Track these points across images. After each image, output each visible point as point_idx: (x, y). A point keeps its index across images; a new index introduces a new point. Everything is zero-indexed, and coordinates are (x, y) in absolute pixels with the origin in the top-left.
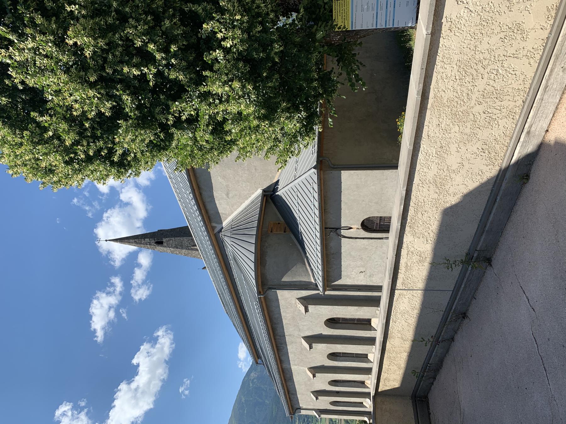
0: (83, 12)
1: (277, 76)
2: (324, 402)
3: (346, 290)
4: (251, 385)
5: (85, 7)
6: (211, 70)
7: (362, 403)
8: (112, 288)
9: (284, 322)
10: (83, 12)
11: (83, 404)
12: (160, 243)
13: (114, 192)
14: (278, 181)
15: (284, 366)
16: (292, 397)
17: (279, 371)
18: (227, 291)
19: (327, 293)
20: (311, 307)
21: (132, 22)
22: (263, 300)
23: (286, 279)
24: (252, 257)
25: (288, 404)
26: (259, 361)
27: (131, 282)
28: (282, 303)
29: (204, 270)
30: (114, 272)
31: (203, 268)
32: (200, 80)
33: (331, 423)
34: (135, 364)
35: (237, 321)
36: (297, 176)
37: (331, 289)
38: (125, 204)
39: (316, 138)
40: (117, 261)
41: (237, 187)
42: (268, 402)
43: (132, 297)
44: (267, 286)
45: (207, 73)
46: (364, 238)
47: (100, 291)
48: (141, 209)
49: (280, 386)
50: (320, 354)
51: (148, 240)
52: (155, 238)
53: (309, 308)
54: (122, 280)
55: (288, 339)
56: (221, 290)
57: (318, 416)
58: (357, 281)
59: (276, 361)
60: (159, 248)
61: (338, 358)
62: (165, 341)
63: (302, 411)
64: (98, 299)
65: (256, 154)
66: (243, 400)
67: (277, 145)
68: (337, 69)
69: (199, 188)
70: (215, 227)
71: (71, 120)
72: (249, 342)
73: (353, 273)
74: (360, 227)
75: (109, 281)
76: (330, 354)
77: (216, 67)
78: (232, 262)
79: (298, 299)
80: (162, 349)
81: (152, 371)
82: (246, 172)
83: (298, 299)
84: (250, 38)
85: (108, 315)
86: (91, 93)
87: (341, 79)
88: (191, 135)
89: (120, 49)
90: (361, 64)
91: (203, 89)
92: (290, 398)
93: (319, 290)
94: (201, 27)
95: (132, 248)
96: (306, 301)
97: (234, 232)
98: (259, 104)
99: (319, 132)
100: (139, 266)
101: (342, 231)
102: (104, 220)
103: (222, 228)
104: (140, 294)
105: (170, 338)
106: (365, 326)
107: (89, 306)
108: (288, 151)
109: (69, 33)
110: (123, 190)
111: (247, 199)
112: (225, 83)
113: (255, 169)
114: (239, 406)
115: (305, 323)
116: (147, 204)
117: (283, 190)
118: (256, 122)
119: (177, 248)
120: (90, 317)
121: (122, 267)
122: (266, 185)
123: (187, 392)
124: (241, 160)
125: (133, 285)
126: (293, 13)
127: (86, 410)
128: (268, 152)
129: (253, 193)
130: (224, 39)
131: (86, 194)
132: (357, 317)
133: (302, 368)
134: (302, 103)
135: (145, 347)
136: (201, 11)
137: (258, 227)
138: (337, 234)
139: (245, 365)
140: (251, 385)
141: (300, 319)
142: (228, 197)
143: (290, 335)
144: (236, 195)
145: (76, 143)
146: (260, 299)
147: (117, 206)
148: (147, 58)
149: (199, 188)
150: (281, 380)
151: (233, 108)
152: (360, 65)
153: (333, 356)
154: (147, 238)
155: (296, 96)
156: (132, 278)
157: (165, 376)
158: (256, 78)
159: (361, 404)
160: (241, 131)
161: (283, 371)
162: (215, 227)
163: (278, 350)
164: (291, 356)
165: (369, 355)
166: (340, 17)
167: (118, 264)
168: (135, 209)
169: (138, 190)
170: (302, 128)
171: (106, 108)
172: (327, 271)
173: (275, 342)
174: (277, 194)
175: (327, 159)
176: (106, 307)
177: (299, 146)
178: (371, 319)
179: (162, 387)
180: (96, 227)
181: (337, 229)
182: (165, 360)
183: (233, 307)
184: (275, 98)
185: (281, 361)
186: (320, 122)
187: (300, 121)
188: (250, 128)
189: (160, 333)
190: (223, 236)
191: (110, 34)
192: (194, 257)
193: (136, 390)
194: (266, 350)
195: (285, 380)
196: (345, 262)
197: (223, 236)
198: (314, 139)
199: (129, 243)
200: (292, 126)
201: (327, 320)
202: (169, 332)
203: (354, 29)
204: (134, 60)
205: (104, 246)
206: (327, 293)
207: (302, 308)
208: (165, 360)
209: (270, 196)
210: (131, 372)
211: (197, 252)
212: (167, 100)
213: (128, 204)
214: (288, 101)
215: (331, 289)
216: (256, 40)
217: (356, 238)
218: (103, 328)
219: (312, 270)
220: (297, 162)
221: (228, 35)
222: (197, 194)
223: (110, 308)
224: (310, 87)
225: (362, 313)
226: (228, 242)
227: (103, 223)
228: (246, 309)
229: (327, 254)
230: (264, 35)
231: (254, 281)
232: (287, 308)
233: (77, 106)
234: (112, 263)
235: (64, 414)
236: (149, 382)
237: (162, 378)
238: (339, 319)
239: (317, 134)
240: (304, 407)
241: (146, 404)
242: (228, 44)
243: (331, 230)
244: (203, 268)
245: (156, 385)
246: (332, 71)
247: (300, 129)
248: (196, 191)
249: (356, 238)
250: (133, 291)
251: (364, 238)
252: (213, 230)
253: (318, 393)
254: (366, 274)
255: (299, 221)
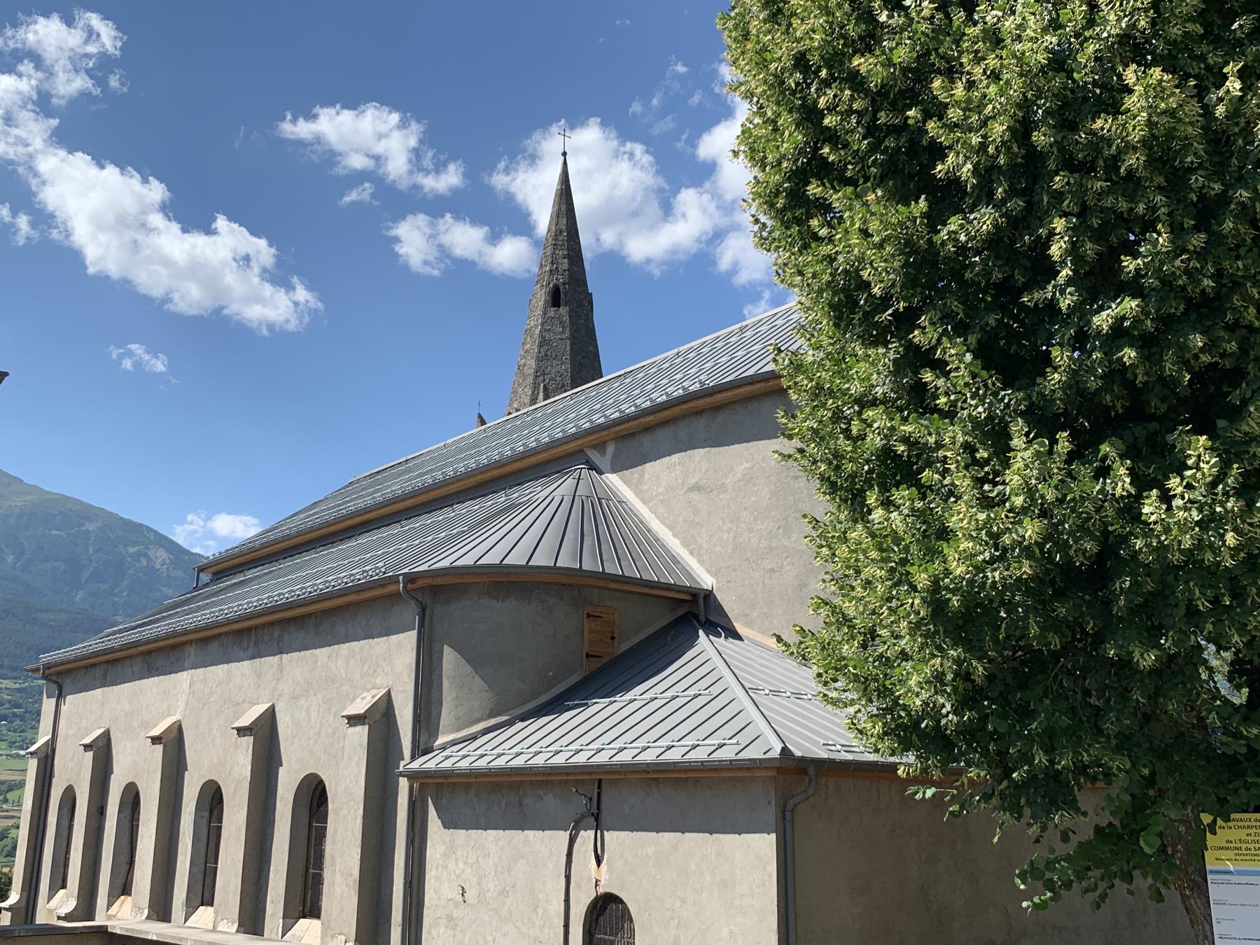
0: (1220, 110)
1: (1055, 642)
2: (74, 770)
3: (410, 841)
4: (132, 550)
5: (1233, 115)
6: (1071, 457)
7: (64, 886)
8: (431, 166)
9: (322, 653)
10: (1220, 110)
11: (114, 82)
12: (555, 298)
13: (703, 173)
14: (738, 637)
15: (191, 651)
16: (98, 672)
17: (175, 634)
18: (418, 483)
19: (404, 783)
20: (362, 732)
21: (1197, 241)
22: (391, 588)
23: (449, 657)
24: (517, 558)
25: (76, 660)
26: (205, 578)
27: (448, 216)
28: (379, 645)
29: (476, 418)
30: (476, 171)
31: (480, 417)
32: (1044, 422)
33: (4, 788)
34: (213, 226)
35: (326, 514)
36: (759, 694)
37: (415, 796)
38: (683, 207)
39: (873, 757)
40: (507, 179)
41: (710, 516)
42: (77, 599)
43: (404, 218)
44: (429, 602)
45: (1064, 443)
46: (567, 901)
47: (424, 132)
48: (647, 246)
49: (133, 636)
50: (222, 760)
51: (566, 266)
52: (569, 285)
53: (358, 728)
54: (455, 191)
55: (271, 661)
56: (418, 467)
57: (32, 749)
58: (437, 878)
59: (207, 627)
60: (540, 297)
61: (206, 814)
62: (274, 307)
63: (53, 701)
64: (403, 125)
65: (828, 577)
66: (90, 527)
67: (853, 638)
68: (1085, 830)
69: (717, 408)
70: (603, 453)
71: (920, 72)
72: (264, 546)
73: (461, 865)
74: (601, 890)
75: (453, 159)
76: (219, 789)
77: (1085, 471)
78: (501, 499)
79: (389, 694)
80: (260, 300)
81: (196, 269)
82: (763, 544)
83: (389, 694)
84: (1170, 572)
85: (356, 152)
86: (998, 129)
87: (1053, 836)
88: (879, 391)
89: (1123, 205)
90: (1104, 896)
91: (1018, 427)
92: (94, 665)
93: (413, 758)
94: (1198, 431)
95: (543, 219)
96: (379, 719)
97: (588, 507)
98: (972, 591)
99: (894, 767)
100: (494, 238)
101: (591, 833)
102: (623, 144)
103: (600, 473)
104: (412, 240)
105: (287, 321)
106: (298, 900)
107: (383, 102)
108: (834, 668)
109: (1156, 72)
110: (706, 197)
111: (685, 545)
112: (1030, 492)
113: (773, 570)
114: (73, 515)
115: (314, 715)
116: (665, 263)
117: (711, 652)
118: (922, 579)
119: (541, 345)
120: (353, 103)
121: (490, 190)
122: (727, 601)
123: (128, 364)
124: (808, 529)
125: (441, 221)
126: (1245, 691)
127: (97, 92)
128: (835, 610)
129: (701, 562)
130: (1166, 498)
131: (696, 99)
132: (327, 874)
133: (181, 703)
134: (984, 719)
135: (261, 249)
136: (1245, 428)
137: (604, 576)
138: (583, 817)
139: (195, 532)
140: (132, 550)
141: (329, 699)
142: (691, 489)
143: (281, 668)
144: (695, 512)
145: (856, 81)
146: (394, 580)
147: (662, 182)
148: (1100, 281)
149: (717, 408)
150: (148, 642)
151: (962, 516)
152: (1099, 891)
153: (212, 798)
154: (570, 264)
155: (1002, 700)
156: (458, 217)
157: (181, 305)
158: (1052, 582)
159: (60, 882)
160: (897, 540)
161: (174, 647)
162: (603, 453)
163: (240, 632)
164: (219, 671)
165: (209, 908)
166: (1242, 834)
167: (499, 180)
168: (653, 228)
169: (704, 238)
170: (909, 714)
171: (957, 165)
172: (468, 786)
173: (263, 625)
174: (701, 632)
175: (812, 789)
176: (379, 148)
177: (852, 703)
178: (318, 917)
179: (147, 300)
180: (604, 124)
181: (597, 819)
182: (223, 308)
183: (369, 501)
184: (995, 640)
185: (206, 641)
186: (925, 770)
187: (930, 710)
188: (904, 562)
189: (302, 294)
190: (576, 474)
191: (1160, 180)
192: (514, 392)
193: (145, 227)
194: (236, 598)
195: (150, 652)
196: (495, 842)
197: (576, 474)
198: (877, 751)
199: (556, 216)
200: (914, 688)
201: (321, 782)
202: (307, 319)
203: (1209, 877)
204: (1089, 245)
205: (552, 144)
206: (404, 783)
207: (359, 707)
208: (223, 308)
209: (693, 614)
210: (191, 213)
211: (527, 400)
212: (982, 329)
213: (667, 209)
214: (990, 678)
215: (415, 796)
216: (1172, 592)
217: (568, 878)
218: (318, 139)
219: (474, 738)
220: (798, 695)
221: (1184, 504)
222: (700, 403)
223: (377, 158)
224: (1031, 739)
225: (338, 890)
226: (562, 488)
227: (615, 143)
228: (364, 539)
229: (520, 784)
230: (1182, 611)
231: (445, 563)
232: (363, 661)
233: (959, 91)
234: (502, 165)
235: (91, 35)
236: (167, 262)
237: (176, 297)
238: (324, 818)
239: (892, 759)
240: (64, 708)
241: (99, 251)
242: (1150, 508)
243: (593, 799)
244: (480, 417)
245: (150, 281)
246: (1077, 810)
247: (905, 707)
248: (708, 400)
249: (568, 878)
250: (422, 219)
251: (567, 901)
252: (594, 447)
253: (102, 751)
254: (457, 905)
255: (622, 699)
